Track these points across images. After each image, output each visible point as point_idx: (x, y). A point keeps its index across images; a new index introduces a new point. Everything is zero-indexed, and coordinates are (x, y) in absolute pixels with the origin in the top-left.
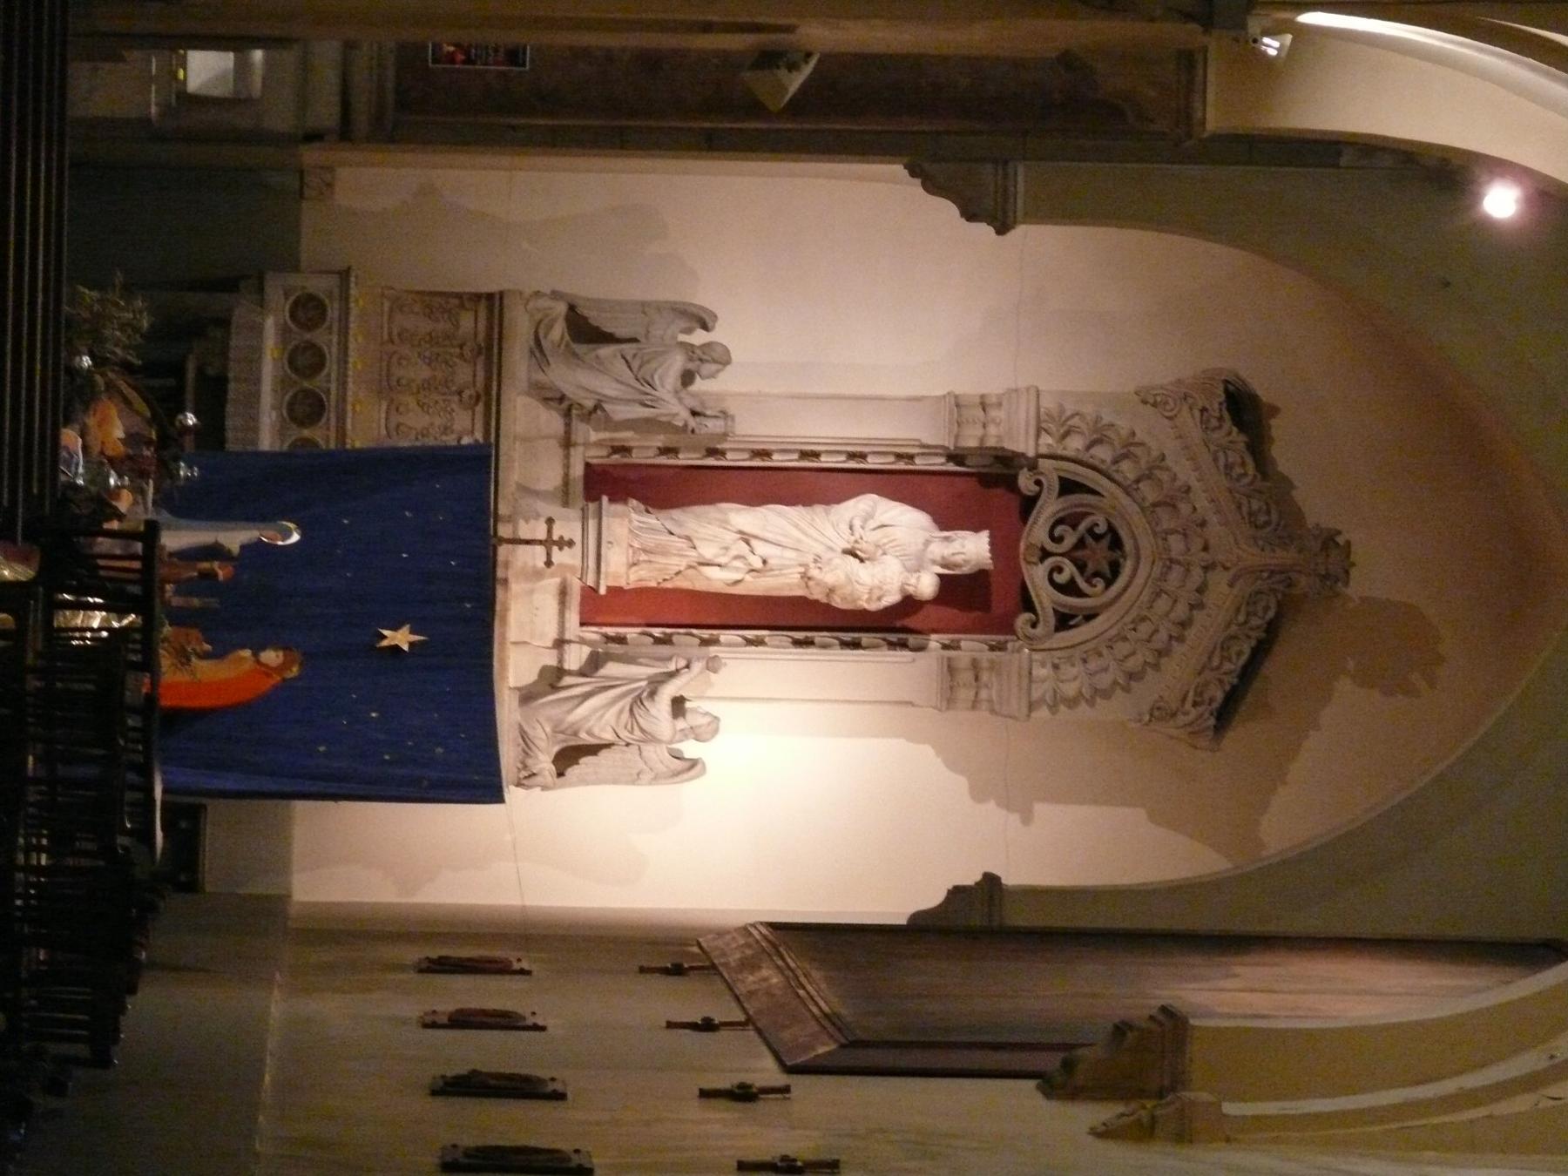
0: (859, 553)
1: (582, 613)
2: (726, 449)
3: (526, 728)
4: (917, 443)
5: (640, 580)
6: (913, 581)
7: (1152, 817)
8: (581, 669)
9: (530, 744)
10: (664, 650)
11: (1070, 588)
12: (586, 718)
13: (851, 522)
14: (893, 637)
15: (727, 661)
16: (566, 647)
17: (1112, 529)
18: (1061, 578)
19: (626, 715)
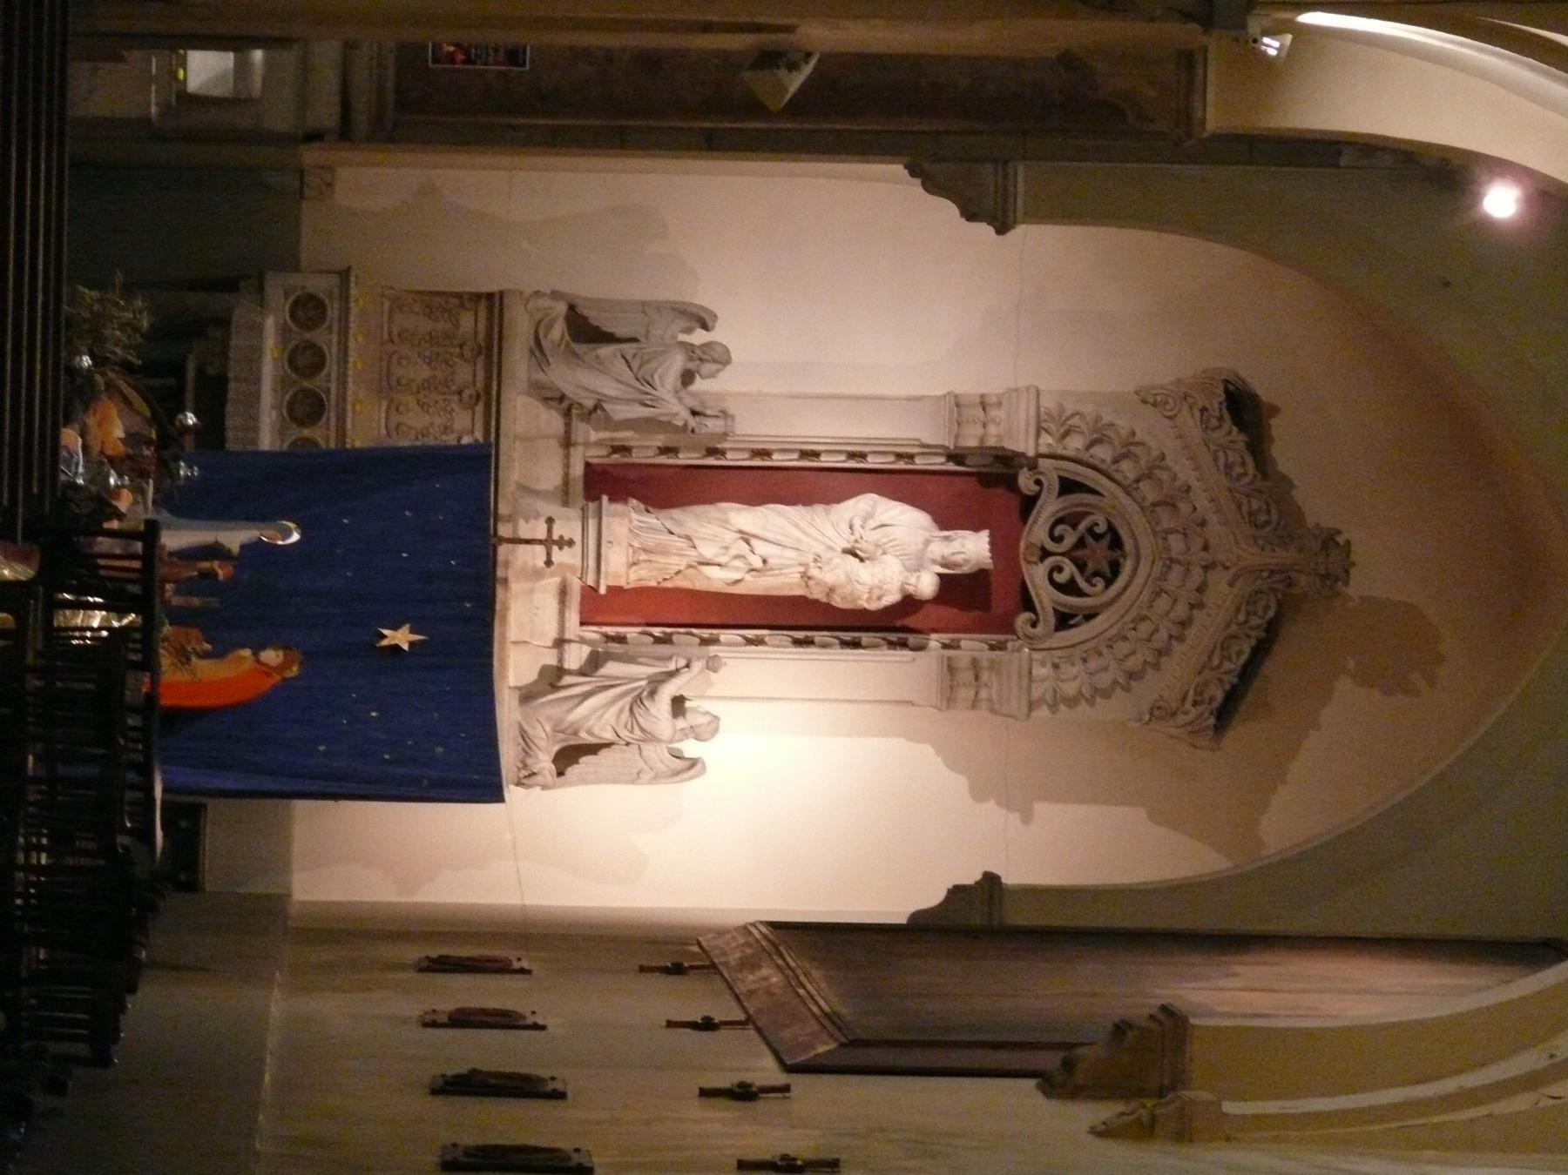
0: (859, 552)
1: (582, 613)
2: (726, 449)
3: (526, 728)
4: (917, 443)
5: (640, 580)
6: (913, 581)
7: (1152, 817)
8: (581, 668)
9: (530, 744)
10: (664, 649)
11: (1070, 588)
12: (586, 718)
13: (851, 521)
14: (893, 637)
15: (727, 660)
16: (566, 646)
17: (1112, 529)
18: (1061, 578)
19: (626, 714)
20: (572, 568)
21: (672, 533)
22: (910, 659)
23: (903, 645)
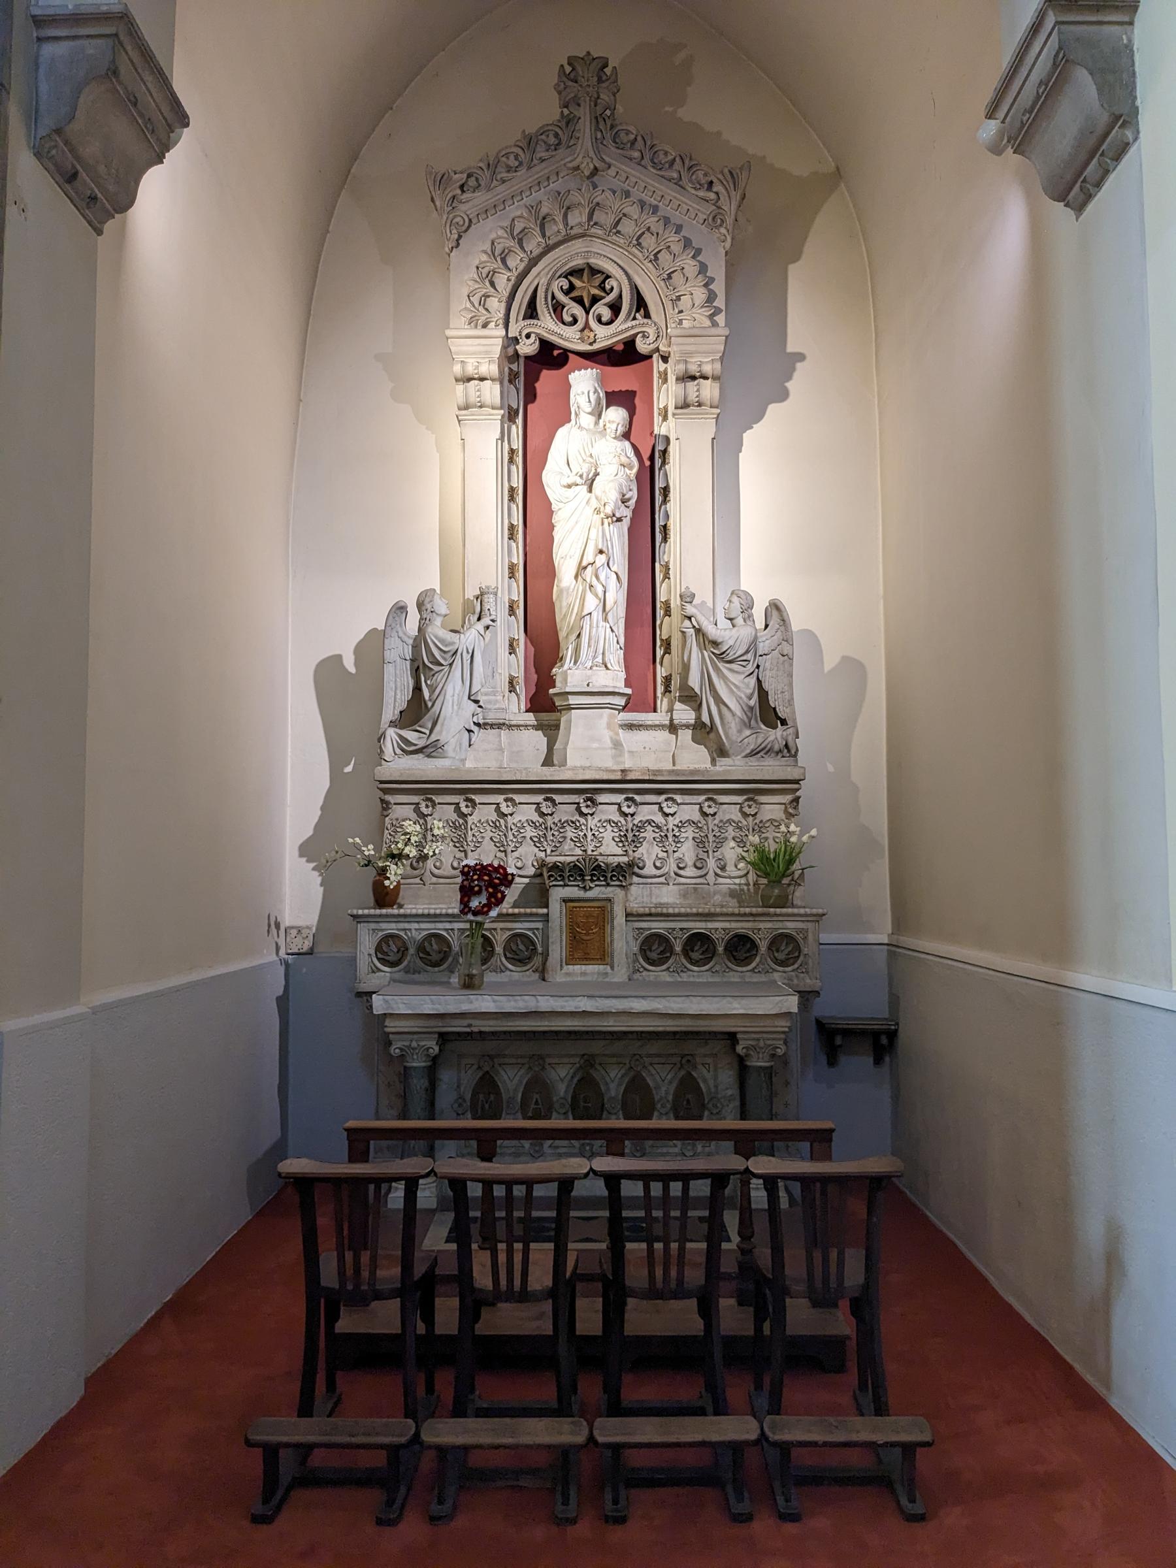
0: (590, 476)
2: (509, 598)
3: (748, 751)
4: (500, 442)
5: (619, 662)
6: (614, 426)
7: (796, 257)
9: (763, 746)
10: (675, 644)
11: (615, 308)
12: (738, 699)
13: (565, 487)
16: (676, 722)
18: (606, 314)
19: (734, 666)
20: (611, 717)
21: (579, 634)
22: (678, 239)
23: (664, 452)
